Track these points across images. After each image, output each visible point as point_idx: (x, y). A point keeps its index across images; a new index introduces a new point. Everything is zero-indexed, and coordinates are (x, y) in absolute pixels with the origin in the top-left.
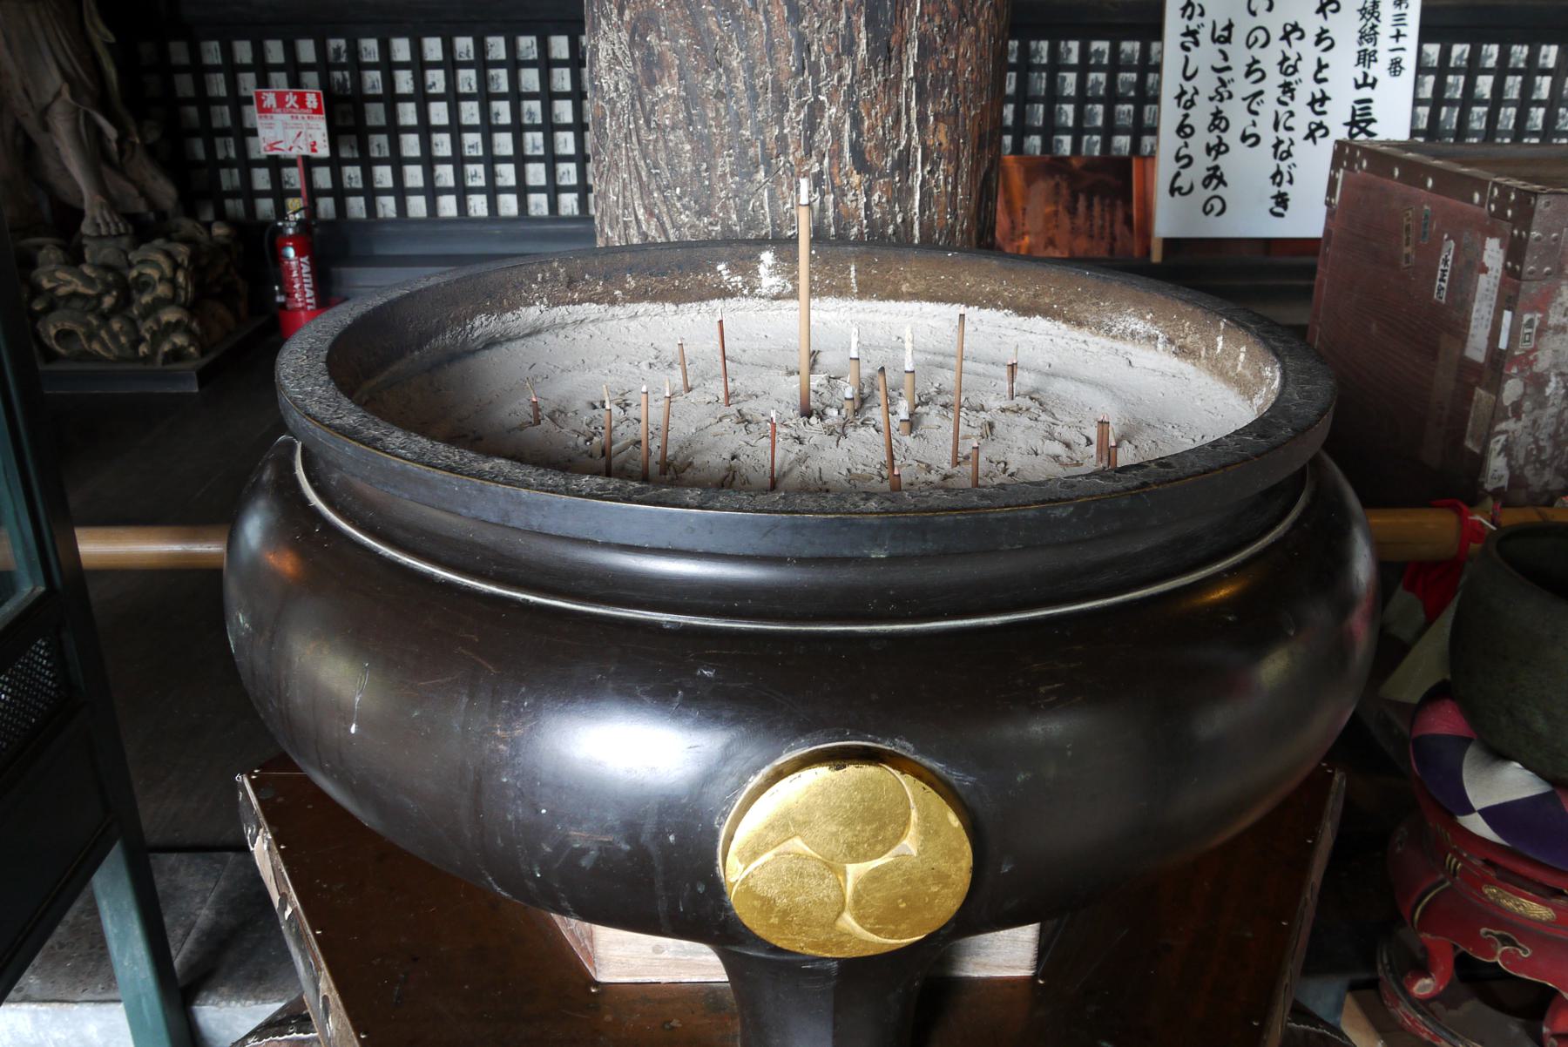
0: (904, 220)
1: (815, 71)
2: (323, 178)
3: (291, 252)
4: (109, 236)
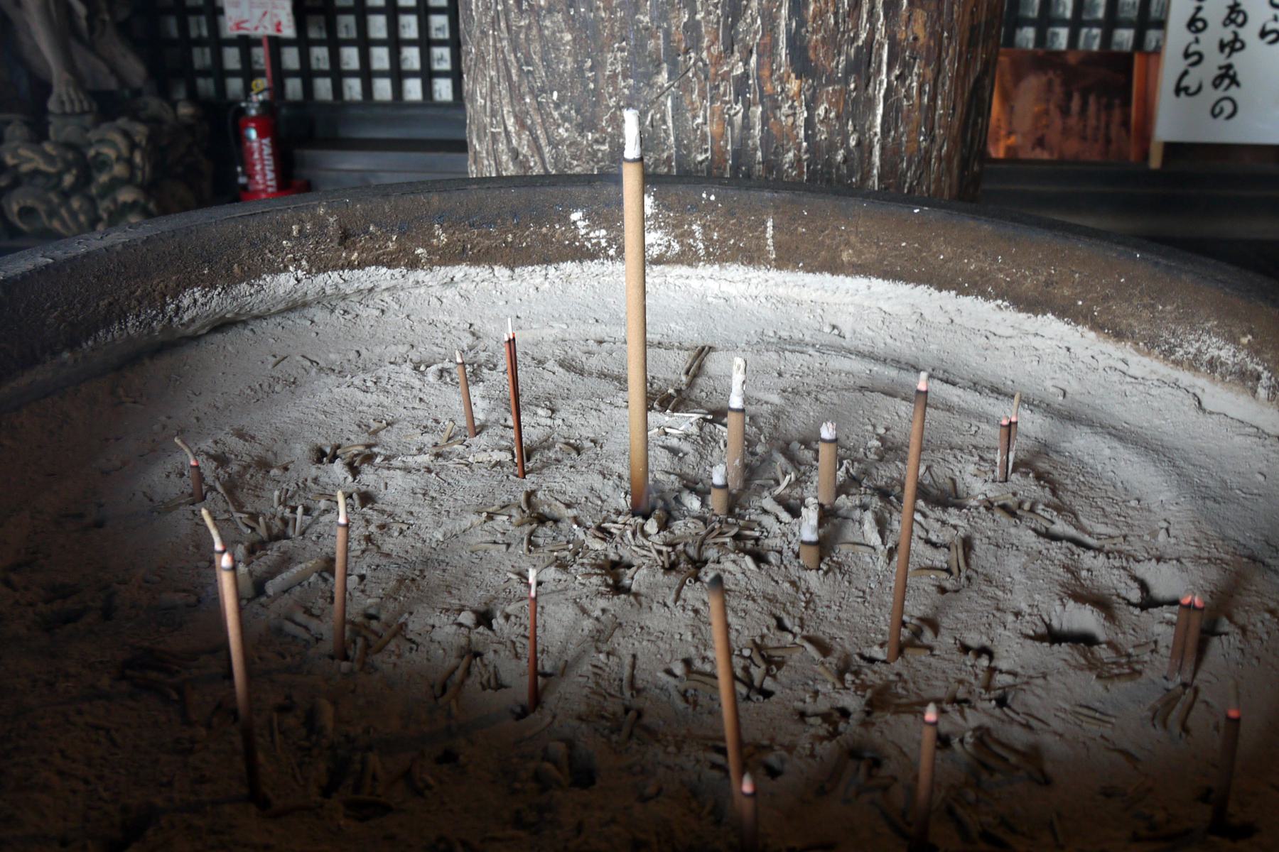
0: (859, 143)
2: (291, 58)
3: (253, 134)
4: (73, 114)
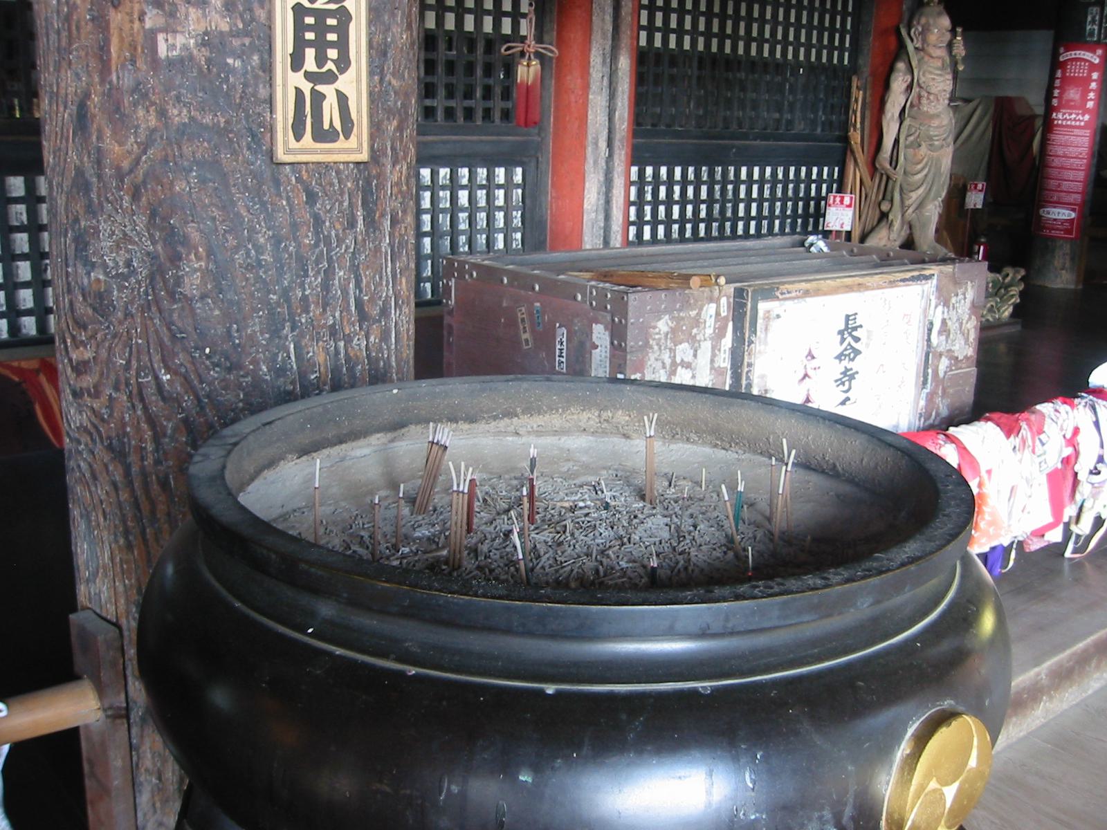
1: (328, 243)
